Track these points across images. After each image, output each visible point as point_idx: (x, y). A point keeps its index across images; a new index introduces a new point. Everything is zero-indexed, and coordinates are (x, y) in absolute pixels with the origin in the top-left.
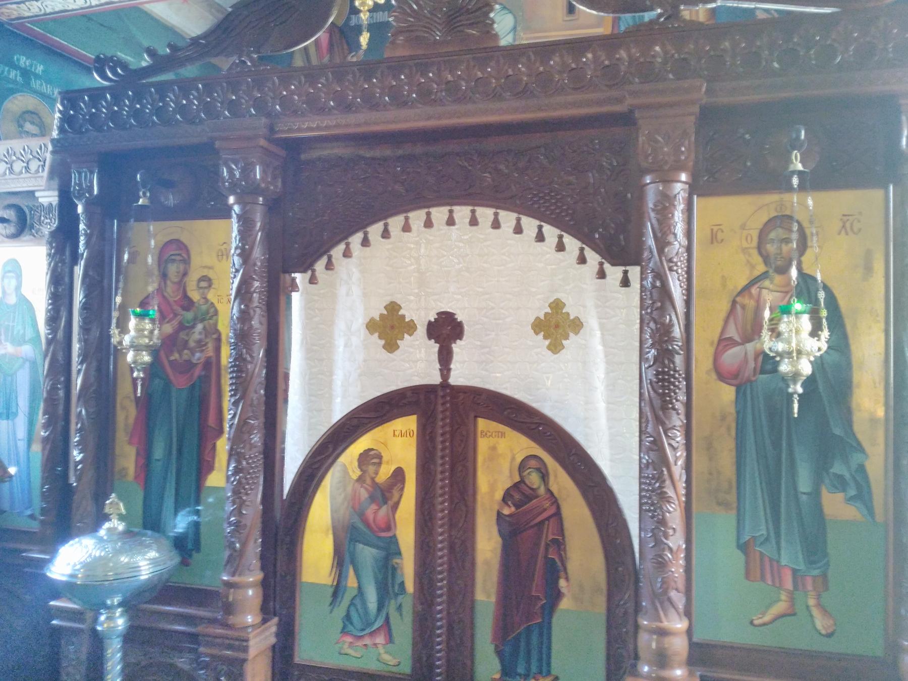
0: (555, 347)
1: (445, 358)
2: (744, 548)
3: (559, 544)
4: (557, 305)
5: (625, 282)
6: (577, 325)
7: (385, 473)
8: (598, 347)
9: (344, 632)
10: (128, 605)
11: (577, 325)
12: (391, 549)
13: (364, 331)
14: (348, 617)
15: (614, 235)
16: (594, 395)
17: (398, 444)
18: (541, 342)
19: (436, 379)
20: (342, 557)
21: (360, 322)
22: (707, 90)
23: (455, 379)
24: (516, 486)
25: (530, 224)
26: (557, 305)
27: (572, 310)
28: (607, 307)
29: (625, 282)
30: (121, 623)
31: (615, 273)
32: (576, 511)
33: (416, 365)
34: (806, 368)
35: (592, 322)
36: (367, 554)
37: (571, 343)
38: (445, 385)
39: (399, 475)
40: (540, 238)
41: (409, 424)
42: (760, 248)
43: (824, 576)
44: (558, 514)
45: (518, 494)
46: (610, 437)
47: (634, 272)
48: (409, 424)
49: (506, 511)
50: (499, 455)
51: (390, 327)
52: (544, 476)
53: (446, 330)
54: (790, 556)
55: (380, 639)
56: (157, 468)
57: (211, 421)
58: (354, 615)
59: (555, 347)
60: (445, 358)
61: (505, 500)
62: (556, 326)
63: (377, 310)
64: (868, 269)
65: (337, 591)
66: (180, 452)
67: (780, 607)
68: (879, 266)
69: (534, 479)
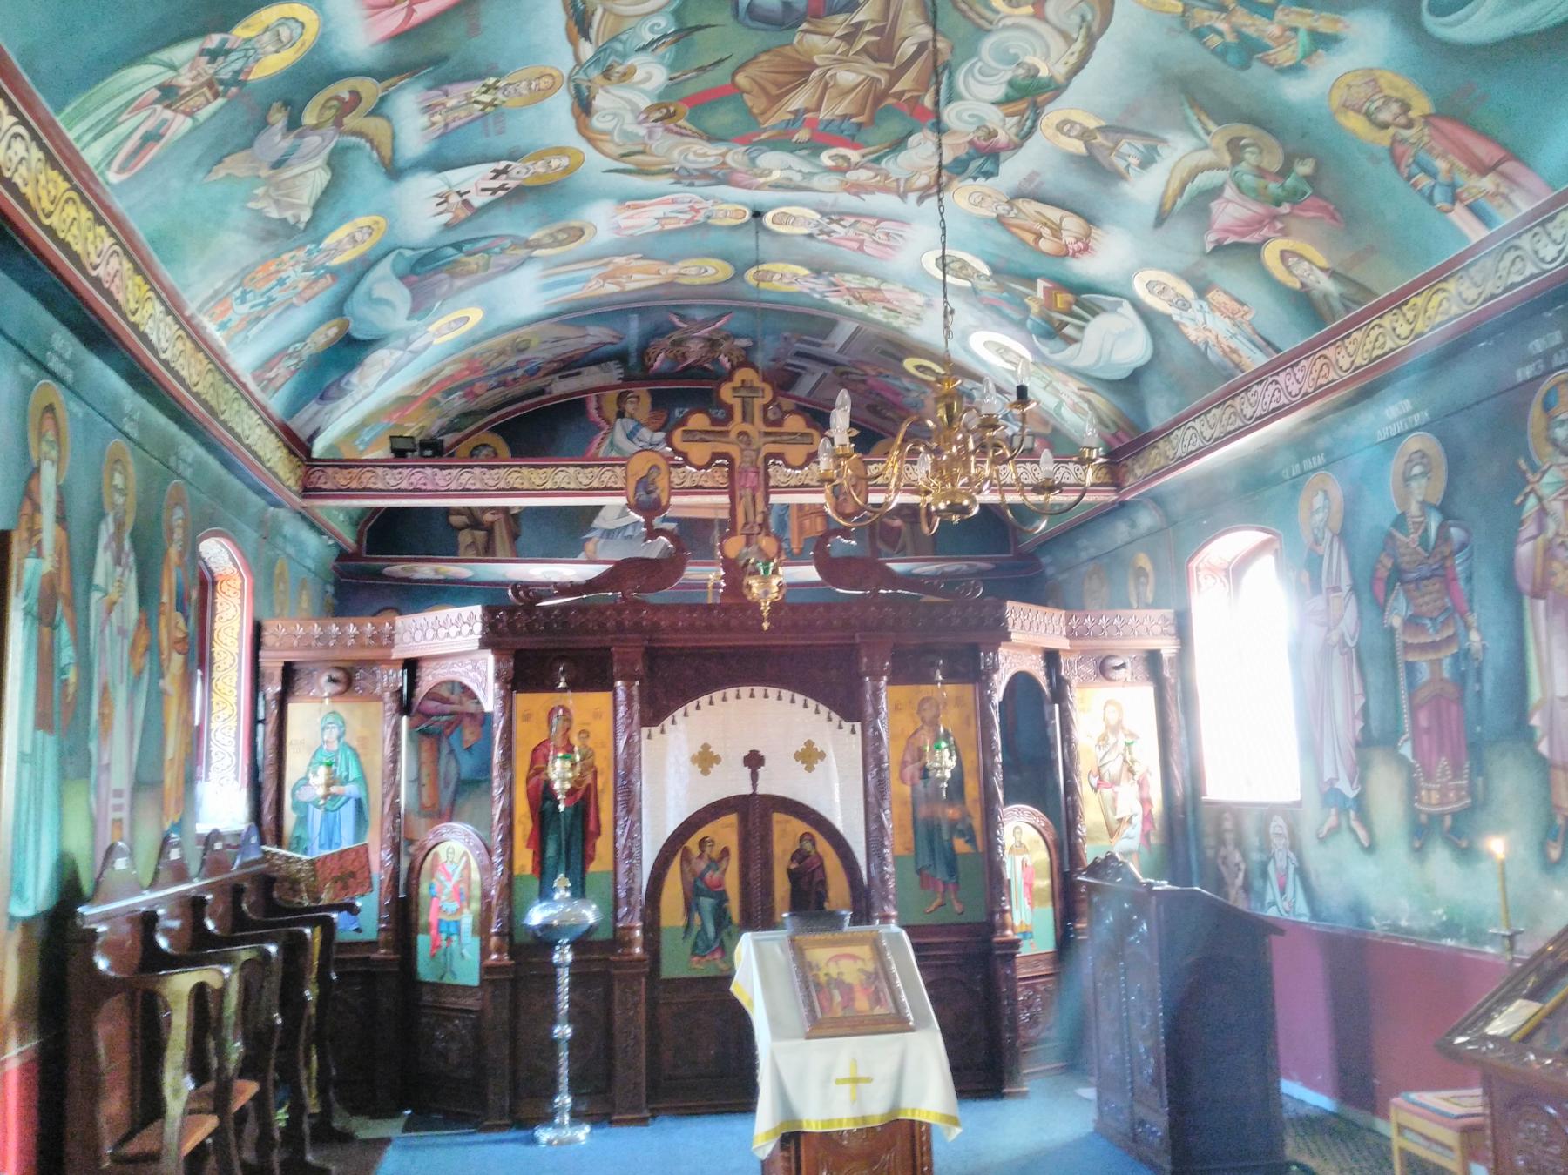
0: (810, 769)
1: (754, 777)
2: (919, 872)
3: (823, 882)
4: (809, 744)
5: (853, 731)
6: (822, 755)
7: (715, 852)
8: (834, 767)
9: (693, 954)
10: (576, 945)
11: (822, 755)
12: (721, 898)
13: (689, 763)
14: (695, 945)
15: (848, 704)
16: (836, 794)
17: (725, 832)
18: (800, 765)
19: (749, 791)
20: (690, 906)
21: (685, 757)
22: (1452, 936)
23: (761, 790)
24: (798, 851)
25: (799, 698)
26: (809, 744)
27: (819, 746)
28: (841, 744)
29: (853, 731)
30: (569, 957)
31: (847, 726)
32: (832, 863)
33: (735, 782)
34: (948, 775)
35: (830, 753)
36: (707, 903)
37: (819, 765)
38: (754, 794)
39: (725, 852)
40: (806, 706)
41: (732, 819)
42: (919, 712)
43: (957, 883)
44: (822, 866)
45: (799, 856)
46: (847, 817)
47: (858, 726)
48: (732, 819)
49: (793, 866)
50: (786, 834)
51: (706, 759)
52: (814, 844)
53: (754, 761)
54: (941, 874)
55: (717, 955)
56: (550, 862)
57: (592, 827)
58: (700, 944)
59: (810, 769)
60: (754, 777)
61: (792, 859)
62: (809, 756)
63: (697, 749)
64: (968, 724)
65: (688, 927)
66: (568, 851)
67: (938, 901)
68: (973, 722)
69: (808, 846)
